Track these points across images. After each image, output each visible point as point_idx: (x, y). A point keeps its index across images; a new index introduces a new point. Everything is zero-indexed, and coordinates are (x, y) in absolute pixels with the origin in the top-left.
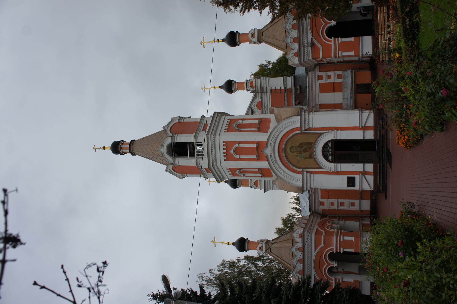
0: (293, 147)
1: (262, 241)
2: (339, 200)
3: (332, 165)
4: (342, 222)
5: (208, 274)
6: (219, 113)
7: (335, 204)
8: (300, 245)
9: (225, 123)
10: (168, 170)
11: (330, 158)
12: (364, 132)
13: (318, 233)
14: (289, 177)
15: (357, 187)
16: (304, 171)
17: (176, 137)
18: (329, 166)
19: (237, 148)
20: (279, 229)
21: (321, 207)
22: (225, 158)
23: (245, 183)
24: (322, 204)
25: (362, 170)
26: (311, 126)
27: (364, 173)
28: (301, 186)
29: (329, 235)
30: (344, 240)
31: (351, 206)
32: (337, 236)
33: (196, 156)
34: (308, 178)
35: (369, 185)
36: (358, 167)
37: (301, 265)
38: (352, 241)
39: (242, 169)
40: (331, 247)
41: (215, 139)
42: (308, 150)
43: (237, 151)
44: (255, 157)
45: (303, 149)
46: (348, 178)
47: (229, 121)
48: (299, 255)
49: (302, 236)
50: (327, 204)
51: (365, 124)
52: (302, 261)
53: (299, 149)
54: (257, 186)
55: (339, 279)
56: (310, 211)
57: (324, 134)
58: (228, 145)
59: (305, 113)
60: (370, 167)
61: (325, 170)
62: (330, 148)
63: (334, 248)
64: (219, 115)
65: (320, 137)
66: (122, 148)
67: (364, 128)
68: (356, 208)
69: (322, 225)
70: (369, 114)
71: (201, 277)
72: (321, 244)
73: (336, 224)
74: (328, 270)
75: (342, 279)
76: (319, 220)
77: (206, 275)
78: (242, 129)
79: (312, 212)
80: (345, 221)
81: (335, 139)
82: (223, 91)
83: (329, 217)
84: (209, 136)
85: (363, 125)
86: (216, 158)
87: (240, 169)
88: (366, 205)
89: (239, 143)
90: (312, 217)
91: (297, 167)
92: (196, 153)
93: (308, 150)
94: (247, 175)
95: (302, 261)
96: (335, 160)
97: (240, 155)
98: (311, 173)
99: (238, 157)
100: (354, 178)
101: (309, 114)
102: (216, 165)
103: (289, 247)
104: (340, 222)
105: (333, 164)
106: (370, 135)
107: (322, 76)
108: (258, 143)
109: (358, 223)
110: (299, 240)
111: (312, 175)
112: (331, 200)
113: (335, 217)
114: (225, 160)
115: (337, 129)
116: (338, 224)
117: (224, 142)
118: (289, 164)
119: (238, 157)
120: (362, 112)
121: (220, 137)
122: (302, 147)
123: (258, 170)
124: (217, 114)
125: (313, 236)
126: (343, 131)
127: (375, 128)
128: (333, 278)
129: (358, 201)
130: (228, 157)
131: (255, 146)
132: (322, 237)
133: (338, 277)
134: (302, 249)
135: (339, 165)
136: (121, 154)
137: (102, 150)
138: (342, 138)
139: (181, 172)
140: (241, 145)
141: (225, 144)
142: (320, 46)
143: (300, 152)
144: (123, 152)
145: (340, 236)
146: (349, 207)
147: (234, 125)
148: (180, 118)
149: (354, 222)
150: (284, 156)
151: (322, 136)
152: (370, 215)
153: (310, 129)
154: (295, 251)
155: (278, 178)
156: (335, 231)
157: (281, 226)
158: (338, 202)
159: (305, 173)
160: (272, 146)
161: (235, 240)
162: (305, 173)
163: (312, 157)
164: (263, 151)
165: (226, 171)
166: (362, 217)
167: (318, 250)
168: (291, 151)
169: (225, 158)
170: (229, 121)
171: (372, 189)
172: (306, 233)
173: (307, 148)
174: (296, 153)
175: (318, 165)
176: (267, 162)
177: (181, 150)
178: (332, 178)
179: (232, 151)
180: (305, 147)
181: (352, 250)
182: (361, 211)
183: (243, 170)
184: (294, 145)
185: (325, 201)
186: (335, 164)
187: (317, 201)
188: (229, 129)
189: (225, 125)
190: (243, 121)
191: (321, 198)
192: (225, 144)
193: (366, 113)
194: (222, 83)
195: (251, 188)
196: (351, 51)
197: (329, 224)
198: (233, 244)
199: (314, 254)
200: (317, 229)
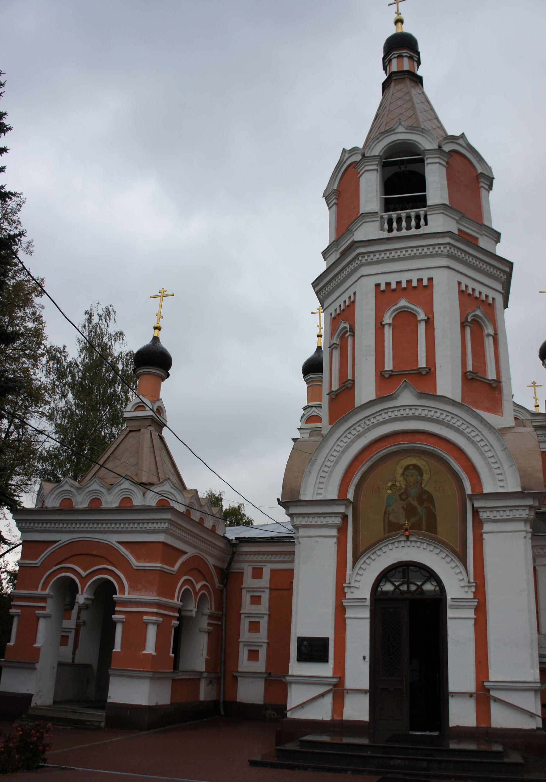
0: (421, 474)
1: (160, 410)
2: (266, 618)
3: (366, 594)
4: (204, 623)
5: (112, 329)
6: (509, 275)
7: (254, 608)
8: (138, 501)
9: (485, 291)
10: (347, 156)
11: (388, 587)
12: (471, 695)
13: (170, 552)
14: (329, 464)
15: (296, 668)
16: (347, 507)
17: (437, 160)
18: (363, 582)
19: (414, 315)
20: (221, 500)
21: (248, 571)
22: (383, 287)
23: (313, 393)
24: (257, 573)
25: (349, 684)
26: (487, 527)
27: (338, 690)
28: (302, 498)
29: (165, 583)
30: (146, 624)
31: (250, 651)
32: (159, 605)
33: (386, 215)
35: (302, 706)
36: (358, 673)
37: (85, 505)
38: (144, 647)
39: (353, 336)
40: (130, 587)
41: (437, 255)
42: (413, 520)
43: (405, 319)
44: (389, 365)
45: (415, 503)
46: (327, 639)
47: (490, 301)
48: (111, 500)
49: (163, 506)
50: (255, 585)
51: (496, 700)
52: (95, 507)
53: (413, 491)
54: (307, 422)
55: (44, 608)
56: (236, 539)
57: (462, 569)
58: (423, 291)
59: (531, 507)
60: (358, 709)
61: (349, 572)
62: (420, 587)
63: (126, 596)
64: (504, 271)
65: (452, 556)
66: (400, 56)
67: (483, 696)
68: (244, 664)
69: (195, 567)
70: (532, 715)
71: (108, 312)
72: (138, 559)
73: (200, 606)
75: (45, 617)
76: (211, 561)
77: (111, 323)
78: (468, 330)
79: (235, 545)
80: (209, 633)
81: (449, 602)
83: (222, 591)
84: (447, 240)
85: (492, 693)
86: (383, 261)
87: (352, 330)
88: (251, 692)
89: (429, 322)
90: (221, 544)
92: (394, 215)
93: (413, 520)
94: (336, 354)
95: (95, 507)
96: (379, 602)
97: (394, 326)
98: (342, 530)
99: (388, 319)
100: (324, 659)
101: (525, 521)
102: (362, 265)
103: (137, 475)
104: (206, 617)
105: (368, 596)
106: (461, 714)
108: (429, 374)
109: (201, 666)
110: (151, 500)
111: (334, 532)
112: (265, 597)
113: (219, 606)
114: (378, 286)
115: (481, 610)
116: (199, 611)
117: (430, 280)
118: (369, 464)
119: (388, 319)
120: (536, 691)
121: (446, 271)
122: (421, 502)
123: (350, 377)
124: (507, 269)
125: (160, 538)
126: (472, 629)
127: (484, 733)
128: (47, 591)
129: (263, 670)
131: (422, 364)
132: (155, 561)
133: (50, 607)
134: (126, 507)
135: (366, 613)
136: (384, 59)
137: (395, 17)
138: (450, 625)
139: (341, 194)
140: (422, 329)
141: (425, 283)
143: (404, 495)
144: (390, 60)
145: (157, 614)
146: (247, 644)
147: (478, 312)
148: (490, 180)
149: (205, 655)
150: (394, 448)
151: (457, 562)
152: (225, 702)
153: (478, 523)
154: (122, 487)
155: (325, 438)
156: (176, 601)
157: (226, 506)
158: (261, 615)
159: (341, 509)
160: (424, 413)
161: (165, 343)
162: (341, 509)
163: (389, 531)
164: (406, 387)
165: (345, 297)
166: (218, 679)
167: (123, 550)
168: (407, 468)
169: (383, 287)
170: (490, 301)
171: (289, 715)
172: (168, 516)
173: (419, 516)
174: (401, 483)
175: (365, 551)
176: (373, 397)
177: (403, 178)
178: (327, 596)
179: (403, 303)
180: (420, 510)
181: (117, 648)
182: (236, 678)
183: (350, 340)
184: (426, 477)
185: (265, 581)
186: (368, 603)
187: (264, 558)
188: (466, 297)
189: (479, 288)
190: (491, 338)
191: (272, 571)
192: (425, 283)
193: (533, 703)
195: (305, 409)
197: (198, 586)
198: (156, 339)
199: (113, 539)
200: (185, 553)
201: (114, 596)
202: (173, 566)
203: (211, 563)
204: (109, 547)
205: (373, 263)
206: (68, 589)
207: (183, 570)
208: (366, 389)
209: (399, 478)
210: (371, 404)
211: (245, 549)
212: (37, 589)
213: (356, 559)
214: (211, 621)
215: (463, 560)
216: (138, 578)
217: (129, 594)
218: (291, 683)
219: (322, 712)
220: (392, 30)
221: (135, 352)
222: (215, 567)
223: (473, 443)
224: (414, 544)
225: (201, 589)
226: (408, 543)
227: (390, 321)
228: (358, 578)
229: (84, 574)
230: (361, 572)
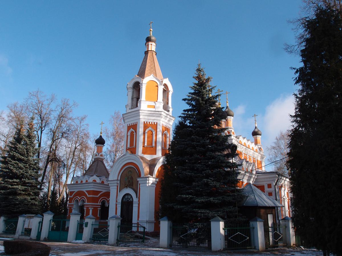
0: (131, 173)
26: (140, 185)
45: (130, 180)
53: (130, 177)
55: (73, 207)
74: (77, 200)
75: (73, 209)
105: (121, 201)
107: (271, 188)
114: (144, 122)
117: (157, 123)
129: (139, 231)
141: (155, 124)
142: (98, 196)
165: (134, 122)
180: (131, 181)
186: (120, 203)
192: (155, 124)
196: (99, 215)
198: (101, 136)
199: (84, 190)
204: (83, 192)
218: (224, 249)
227: (130, 134)
228: (119, 198)
229: (80, 198)
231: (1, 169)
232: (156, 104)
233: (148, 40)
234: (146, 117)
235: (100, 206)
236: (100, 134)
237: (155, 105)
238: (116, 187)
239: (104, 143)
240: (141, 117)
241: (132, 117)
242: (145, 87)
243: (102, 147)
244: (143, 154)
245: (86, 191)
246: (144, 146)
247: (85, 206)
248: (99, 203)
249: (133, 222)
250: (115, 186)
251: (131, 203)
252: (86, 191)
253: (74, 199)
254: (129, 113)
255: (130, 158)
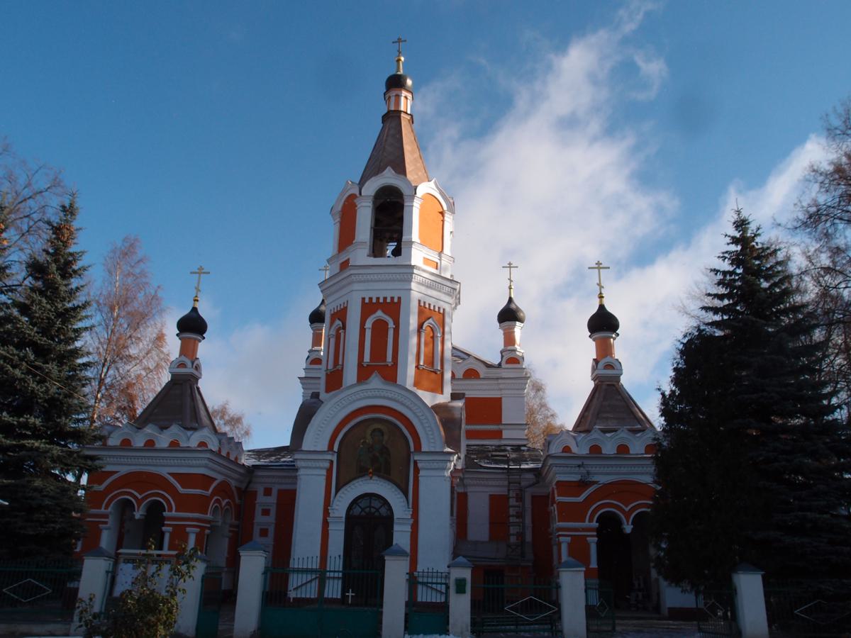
13: (205, 481)
21: (261, 491)
22: (367, 301)
26: (422, 473)
34: (318, 464)
45: (378, 454)
55: (106, 523)
63: (174, 513)
65: (399, 491)
69: (223, 489)
75: (109, 529)
76: (233, 483)
81: (395, 521)
82: (502, 304)
87: (344, 327)
91: (346, 434)
96: (352, 521)
105: (344, 516)
114: (363, 299)
117: (399, 298)
119: (369, 324)
129: (419, 599)
130: (368, 307)
136: (385, 94)
141: (396, 300)
151: (401, 495)
153: (417, 470)
156: (209, 516)
162: (329, 457)
165: (341, 301)
168: (374, 431)
169: (367, 301)
174: (369, 440)
184: (386, 437)
185: (272, 499)
186: (344, 520)
192: (396, 300)
194: (520, 303)
197: (224, 503)
199: (164, 472)
200: (215, 479)
201: (164, 513)
202: (208, 490)
203: (234, 485)
205: (360, 282)
206: (126, 506)
207: (213, 494)
208: (350, 375)
209: (368, 437)
210: (352, 386)
211: (260, 473)
212: (100, 508)
213: (337, 490)
214: (232, 529)
215: (406, 493)
216: (185, 503)
217: (176, 511)
219: (311, 592)
220: (393, 72)
221: (178, 332)
222: (236, 487)
223: (418, 417)
224: (375, 482)
225: (226, 505)
226: (372, 481)
228: (343, 495)
230: (346, 492)
231: (2, 363)
232: (440, 260)
233: (395, 83)
234: (423, 289)
235: (164, 525)
236: (193, 302)
237: (439, 262)
238: (324, 472)
239: (204, 331)
240: (413, 285)
241: (386, 281)
242: (371, 204)
243: (197, 342)
244: (415, 388)
245: (170, 474)
246: (417, 367)
247: (166, 522)
248: (103, 508)
249: (694, 606)
250: (321, 468)
251: (387, 521)
252: (170, 474)
253: (158, 495)
254: (374, 268)
255: (376, 392)
